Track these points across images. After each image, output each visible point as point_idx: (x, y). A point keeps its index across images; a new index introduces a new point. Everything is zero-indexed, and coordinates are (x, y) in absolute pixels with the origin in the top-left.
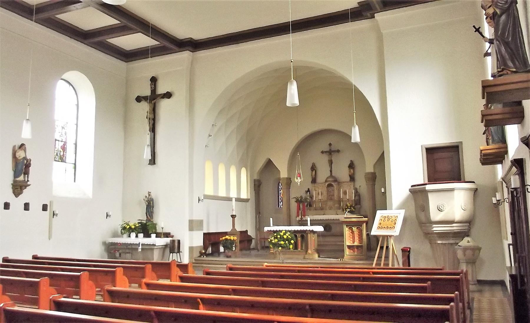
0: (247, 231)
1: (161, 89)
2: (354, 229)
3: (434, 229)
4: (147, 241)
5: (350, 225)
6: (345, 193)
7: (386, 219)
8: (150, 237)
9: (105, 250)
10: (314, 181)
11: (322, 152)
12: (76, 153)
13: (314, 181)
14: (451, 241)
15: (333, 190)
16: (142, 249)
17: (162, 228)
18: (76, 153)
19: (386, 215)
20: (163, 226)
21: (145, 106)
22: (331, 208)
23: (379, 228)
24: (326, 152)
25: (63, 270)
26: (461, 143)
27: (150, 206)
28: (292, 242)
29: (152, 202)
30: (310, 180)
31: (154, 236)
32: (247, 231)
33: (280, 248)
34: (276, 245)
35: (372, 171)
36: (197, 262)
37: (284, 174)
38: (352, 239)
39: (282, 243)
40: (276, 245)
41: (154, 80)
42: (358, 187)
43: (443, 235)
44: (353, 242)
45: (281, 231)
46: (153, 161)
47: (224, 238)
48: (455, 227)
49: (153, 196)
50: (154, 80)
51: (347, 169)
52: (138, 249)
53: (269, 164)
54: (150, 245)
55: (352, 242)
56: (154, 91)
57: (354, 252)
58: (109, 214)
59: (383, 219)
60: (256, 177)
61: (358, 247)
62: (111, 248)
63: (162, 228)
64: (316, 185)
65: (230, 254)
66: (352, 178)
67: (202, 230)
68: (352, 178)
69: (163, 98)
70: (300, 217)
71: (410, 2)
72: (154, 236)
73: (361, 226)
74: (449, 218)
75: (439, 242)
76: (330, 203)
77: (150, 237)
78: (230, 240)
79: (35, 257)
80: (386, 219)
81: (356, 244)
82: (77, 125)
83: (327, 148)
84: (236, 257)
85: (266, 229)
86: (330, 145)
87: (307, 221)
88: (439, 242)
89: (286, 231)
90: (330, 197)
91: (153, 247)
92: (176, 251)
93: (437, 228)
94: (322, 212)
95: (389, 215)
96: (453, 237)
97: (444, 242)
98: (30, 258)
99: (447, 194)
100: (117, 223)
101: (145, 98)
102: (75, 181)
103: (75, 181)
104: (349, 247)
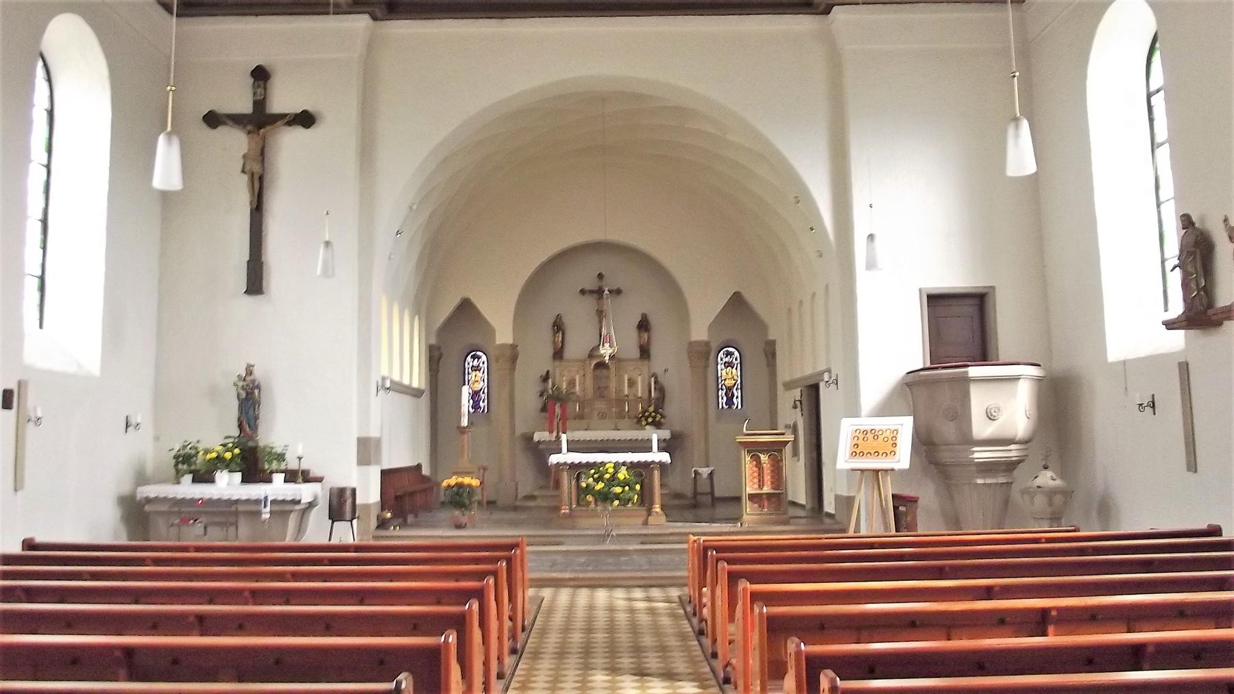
0: (419, 467)
1: (282, 101)
2: (764, 458)
3: (976, 455)
4: (256, 491)
5: (755, 449)
6: (632, 383)
7: (870, 436)
8: (269, 481)
9: (123, 517)
10: (558, 354)
11: (583, 292)
12: (44, 248)
13: (558, 354)
14: (1001, 480)
15: (607, 377)
16: (271, 512)
17: (300, 458)
18: (44, 248)
19: (869, 428)
20: (300, 453)
21: (236, 141)
22: (603, 416)
23: (854, 454)
24: (592, 292)
25: (296, 577)
26: (993, 288)
27: (250, 401)
28: (638, 487)
29: (256, 391)
30: (550, 352)
31: (279, 478)
32: (419, 467)
33: (616, 502)
34: (605, 497)
35: (510, 341)
36: (684, 538)
37: (504, 335)
38: (756, 480)
39: (618, 490)
40: (605, 497)
41: (261, 75)
42: (658, 370)
43: (988, 468)
44: (761, 487)
45: (603, 464)
46: (255, 283)
47: (453, 481)
48: (1013, 452)
49: (258, 374)
50: (261, 75)
51: (633, 333)
52: (259, 513)
53: (466, 308)
54: (283, 502)
55: (756, 486)
56: (260, 104)
57: (761, 506)
58: (133, 421)
59: (861, 436)
60: (433, 341)
61: (769, 495)
62: (136, 512)
63: (300, 458)
64: (563, 363)
65: (464, 520)
66: (645, 352)
67: (378, 462)
68: (645, 352)
69: (289, 124)
70: (555, 434)
71: (251, 5)
72: (279, 478)
73: (780, 451)
74: (1007, 433)
75: (980, 481)
76: (600, 405)
77: (269, 481)
78: (469, 486)
79: (29, 544)
80: (870, 436)
81: (767, 489)
82: (48, 167)
83: (591, 284)
84: (474, 527)
85: (554, 459)
86: (600, 276)
87: (650, 441)
88: (980, 481)
89: (617, 466)
90: (601, 391)
91: (287, 508)
92: (348, 515)
93: (982, 454)
94: (584, 423)
95: (877, 428)
96: (1004, 471)
97: (988, 481)
98: (16, 549)
99: (1007, 387)
100: (148, 448)
101: (237, 120)
102: (41, 327)
103: (41, 327)
104: (752, 497)
